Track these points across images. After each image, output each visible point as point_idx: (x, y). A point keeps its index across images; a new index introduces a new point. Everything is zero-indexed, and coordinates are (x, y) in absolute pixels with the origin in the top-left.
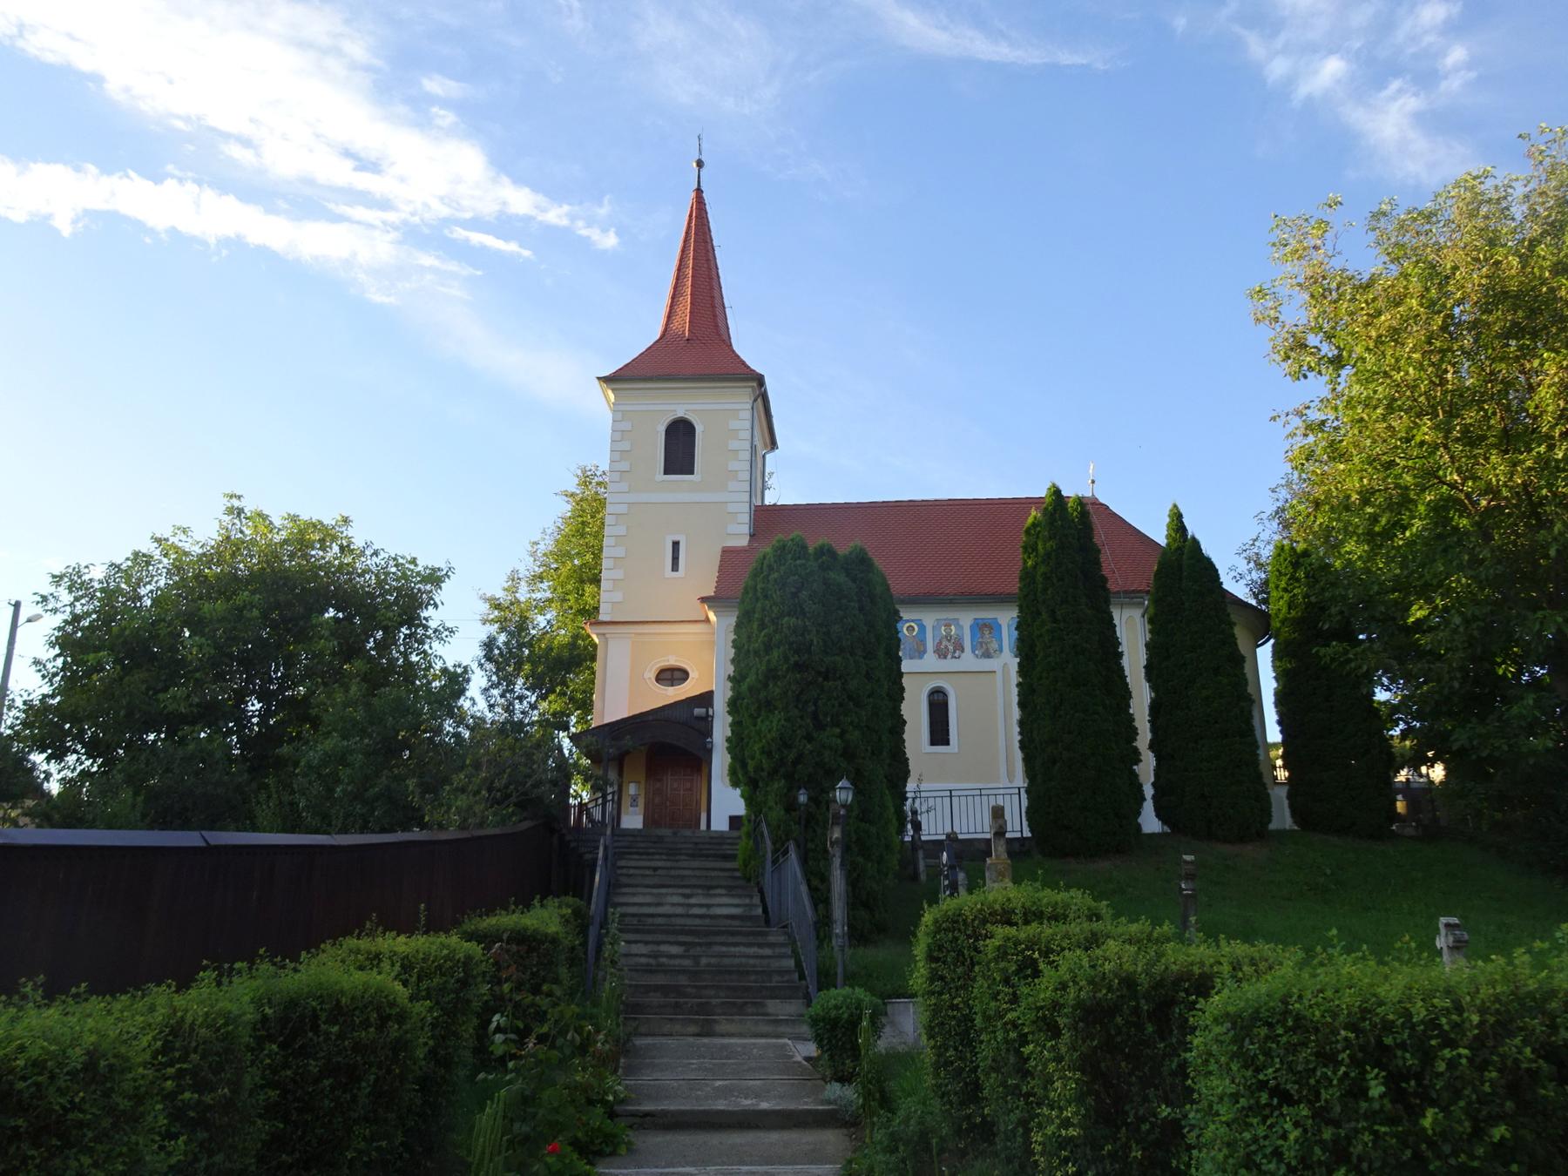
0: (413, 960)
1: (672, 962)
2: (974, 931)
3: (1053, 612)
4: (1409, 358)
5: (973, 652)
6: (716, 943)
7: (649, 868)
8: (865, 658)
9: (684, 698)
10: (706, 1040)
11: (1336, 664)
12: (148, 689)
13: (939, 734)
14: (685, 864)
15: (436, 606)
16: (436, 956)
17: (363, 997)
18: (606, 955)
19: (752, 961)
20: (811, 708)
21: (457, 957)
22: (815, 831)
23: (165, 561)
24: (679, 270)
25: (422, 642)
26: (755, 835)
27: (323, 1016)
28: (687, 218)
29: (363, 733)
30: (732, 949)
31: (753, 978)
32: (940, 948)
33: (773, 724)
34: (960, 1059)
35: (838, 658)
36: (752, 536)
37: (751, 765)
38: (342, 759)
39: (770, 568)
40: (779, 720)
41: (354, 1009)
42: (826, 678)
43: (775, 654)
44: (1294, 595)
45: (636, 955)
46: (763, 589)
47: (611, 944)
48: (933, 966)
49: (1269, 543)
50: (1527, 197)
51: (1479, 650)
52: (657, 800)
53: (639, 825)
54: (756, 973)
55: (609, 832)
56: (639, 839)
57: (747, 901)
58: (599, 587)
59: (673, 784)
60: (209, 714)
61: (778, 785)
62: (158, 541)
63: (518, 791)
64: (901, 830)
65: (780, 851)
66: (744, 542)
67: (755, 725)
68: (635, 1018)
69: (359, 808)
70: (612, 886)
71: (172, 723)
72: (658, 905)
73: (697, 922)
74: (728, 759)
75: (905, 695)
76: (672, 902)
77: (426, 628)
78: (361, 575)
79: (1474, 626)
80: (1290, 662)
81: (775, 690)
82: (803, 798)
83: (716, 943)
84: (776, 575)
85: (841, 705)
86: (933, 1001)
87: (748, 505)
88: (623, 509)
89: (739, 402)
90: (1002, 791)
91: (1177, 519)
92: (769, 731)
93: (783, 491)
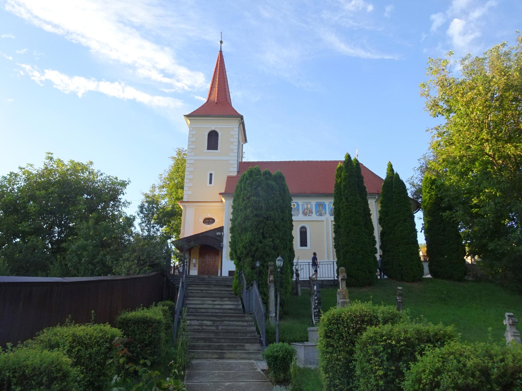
0: (84, 339)
1: (208, 328)
2: (347, 325)
3: (347, 198)
4: (478, 108)
5: (316, 214)
6: (225, 320)
7: (199, 290)
8: (281, 212)
9: (213, 229)
10: (221, 361)
11: (448, 218)
12: (15, 222)
13: (304, 243)
14: (213, 289)
15: (123, 194)
16: (96, 337)
17: (40, 369)
18: (181, 326)
19: (239, 328)
20: (261, 231)
21: (107, 336)
22: (262, 277)
23: (24, 176)
24: (213, 79)
25: (118, 207)
26: (239, 277)
27: (14, 380)
28: (216, 61)
29: (93, 238)
30: (231, 323)
31: (240, 334)
32: (331, 331)
33: (247, 237)
34: (341, 384)
35: (272, 213)
36: (238, 172)
37: (238, 252)
38: (84, 248)
39: (247, 178)
40: (250, 235)
41: (33, 376)
42: (267, 220)
43: (248, 210)
44: (432, 194)
45: (193, 325)
46: (244, 186)
47: (183, 322)
48: (328, 340)
49: (417, 178)
50: (516, 55)
51: (499, 215)
52: (203, 265)
53: (196, 274)
54: (241, 332)
55: (184, 276)
56: (196, 279)
57: (236, 303)
58: (183, 190)
59: (209, 259)
60: (38, 231)
61: (249, 259)
62: (21, 168)
63: (149, 261)
64: (292, 277)
65: (250, 285)
66: (235, 174)
67: (240, 237)
68: (192, 352)
69: (90, 267)
70: (185, 297)
71: (24, 235)
72: (202, 304)
73: (218, 311)
74: (229, 250)
75: (293, 228)
76: (208, 304)
77: (120, 202)
78: (97, 183)
79: (498, 205)
80: (430, 218)
81: (248, 224)
82: (258, 264)
83: (225, 320)
84: (249, 181)
85: (272, 230)
86: (328, 356)
87: (237, 161)
88: (192, 162)
89: (233, 125)
90: (325, 263)
91: (390, 167)
92: (246, 239)
93: (247, 158)
